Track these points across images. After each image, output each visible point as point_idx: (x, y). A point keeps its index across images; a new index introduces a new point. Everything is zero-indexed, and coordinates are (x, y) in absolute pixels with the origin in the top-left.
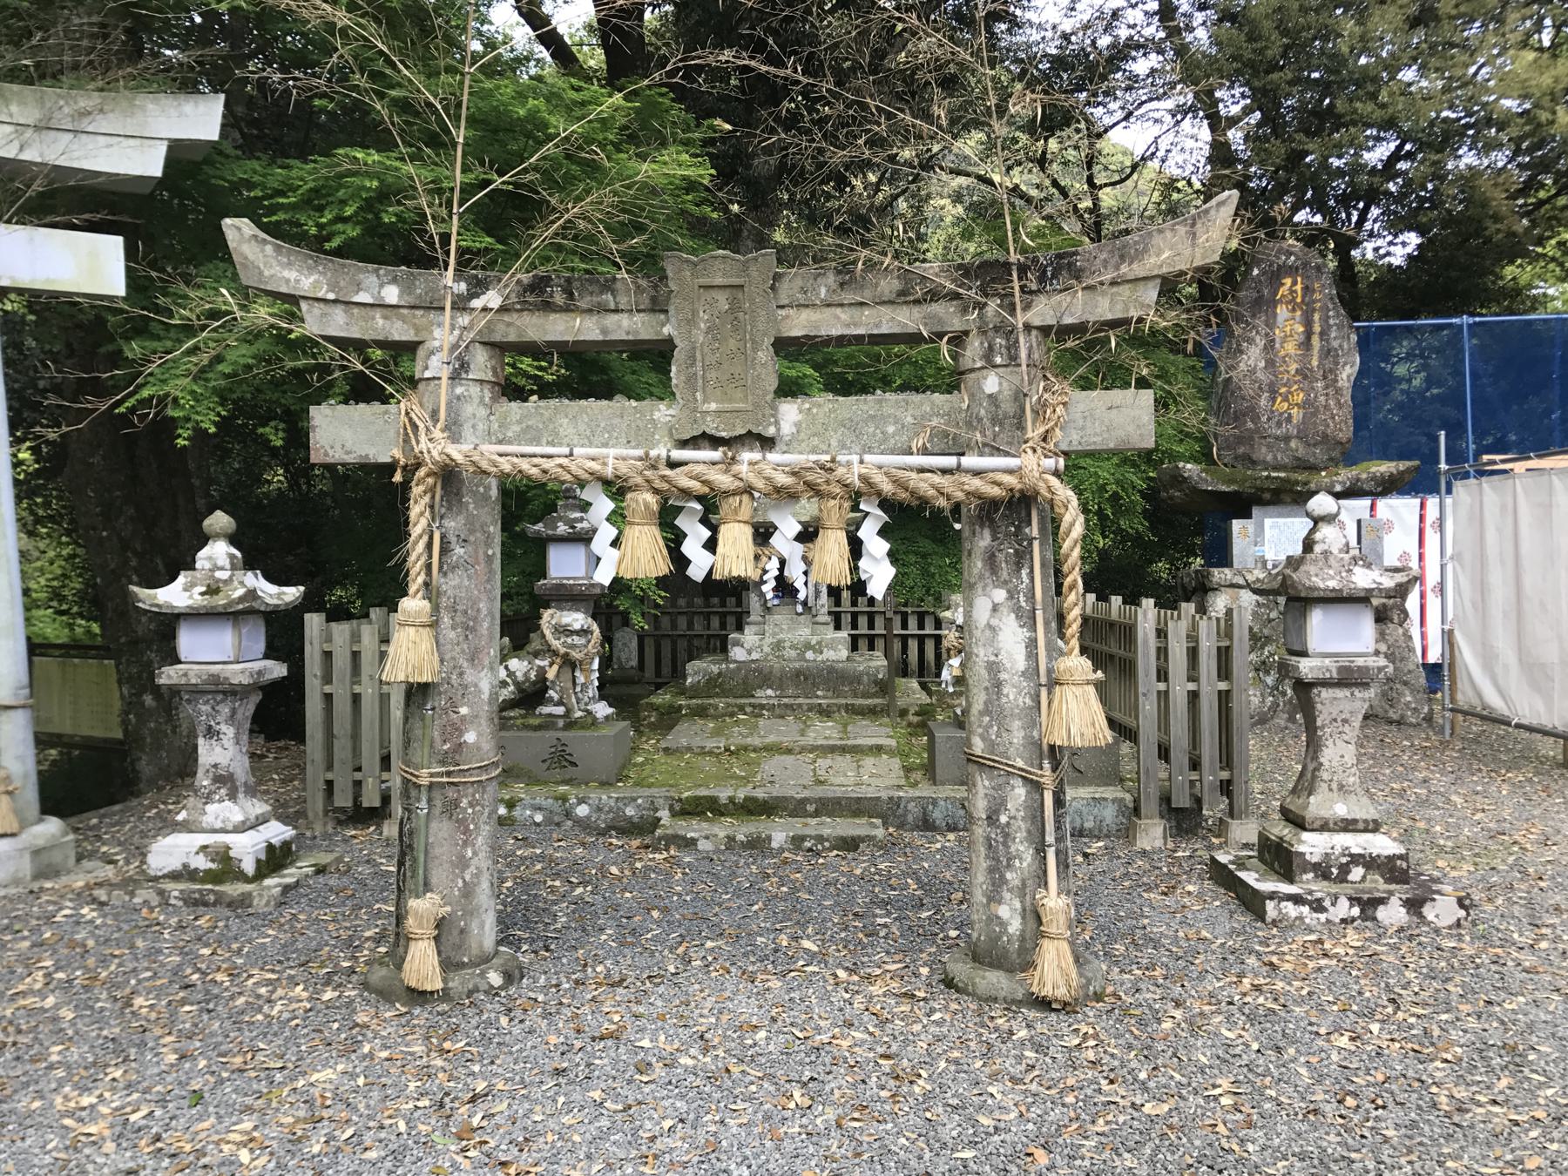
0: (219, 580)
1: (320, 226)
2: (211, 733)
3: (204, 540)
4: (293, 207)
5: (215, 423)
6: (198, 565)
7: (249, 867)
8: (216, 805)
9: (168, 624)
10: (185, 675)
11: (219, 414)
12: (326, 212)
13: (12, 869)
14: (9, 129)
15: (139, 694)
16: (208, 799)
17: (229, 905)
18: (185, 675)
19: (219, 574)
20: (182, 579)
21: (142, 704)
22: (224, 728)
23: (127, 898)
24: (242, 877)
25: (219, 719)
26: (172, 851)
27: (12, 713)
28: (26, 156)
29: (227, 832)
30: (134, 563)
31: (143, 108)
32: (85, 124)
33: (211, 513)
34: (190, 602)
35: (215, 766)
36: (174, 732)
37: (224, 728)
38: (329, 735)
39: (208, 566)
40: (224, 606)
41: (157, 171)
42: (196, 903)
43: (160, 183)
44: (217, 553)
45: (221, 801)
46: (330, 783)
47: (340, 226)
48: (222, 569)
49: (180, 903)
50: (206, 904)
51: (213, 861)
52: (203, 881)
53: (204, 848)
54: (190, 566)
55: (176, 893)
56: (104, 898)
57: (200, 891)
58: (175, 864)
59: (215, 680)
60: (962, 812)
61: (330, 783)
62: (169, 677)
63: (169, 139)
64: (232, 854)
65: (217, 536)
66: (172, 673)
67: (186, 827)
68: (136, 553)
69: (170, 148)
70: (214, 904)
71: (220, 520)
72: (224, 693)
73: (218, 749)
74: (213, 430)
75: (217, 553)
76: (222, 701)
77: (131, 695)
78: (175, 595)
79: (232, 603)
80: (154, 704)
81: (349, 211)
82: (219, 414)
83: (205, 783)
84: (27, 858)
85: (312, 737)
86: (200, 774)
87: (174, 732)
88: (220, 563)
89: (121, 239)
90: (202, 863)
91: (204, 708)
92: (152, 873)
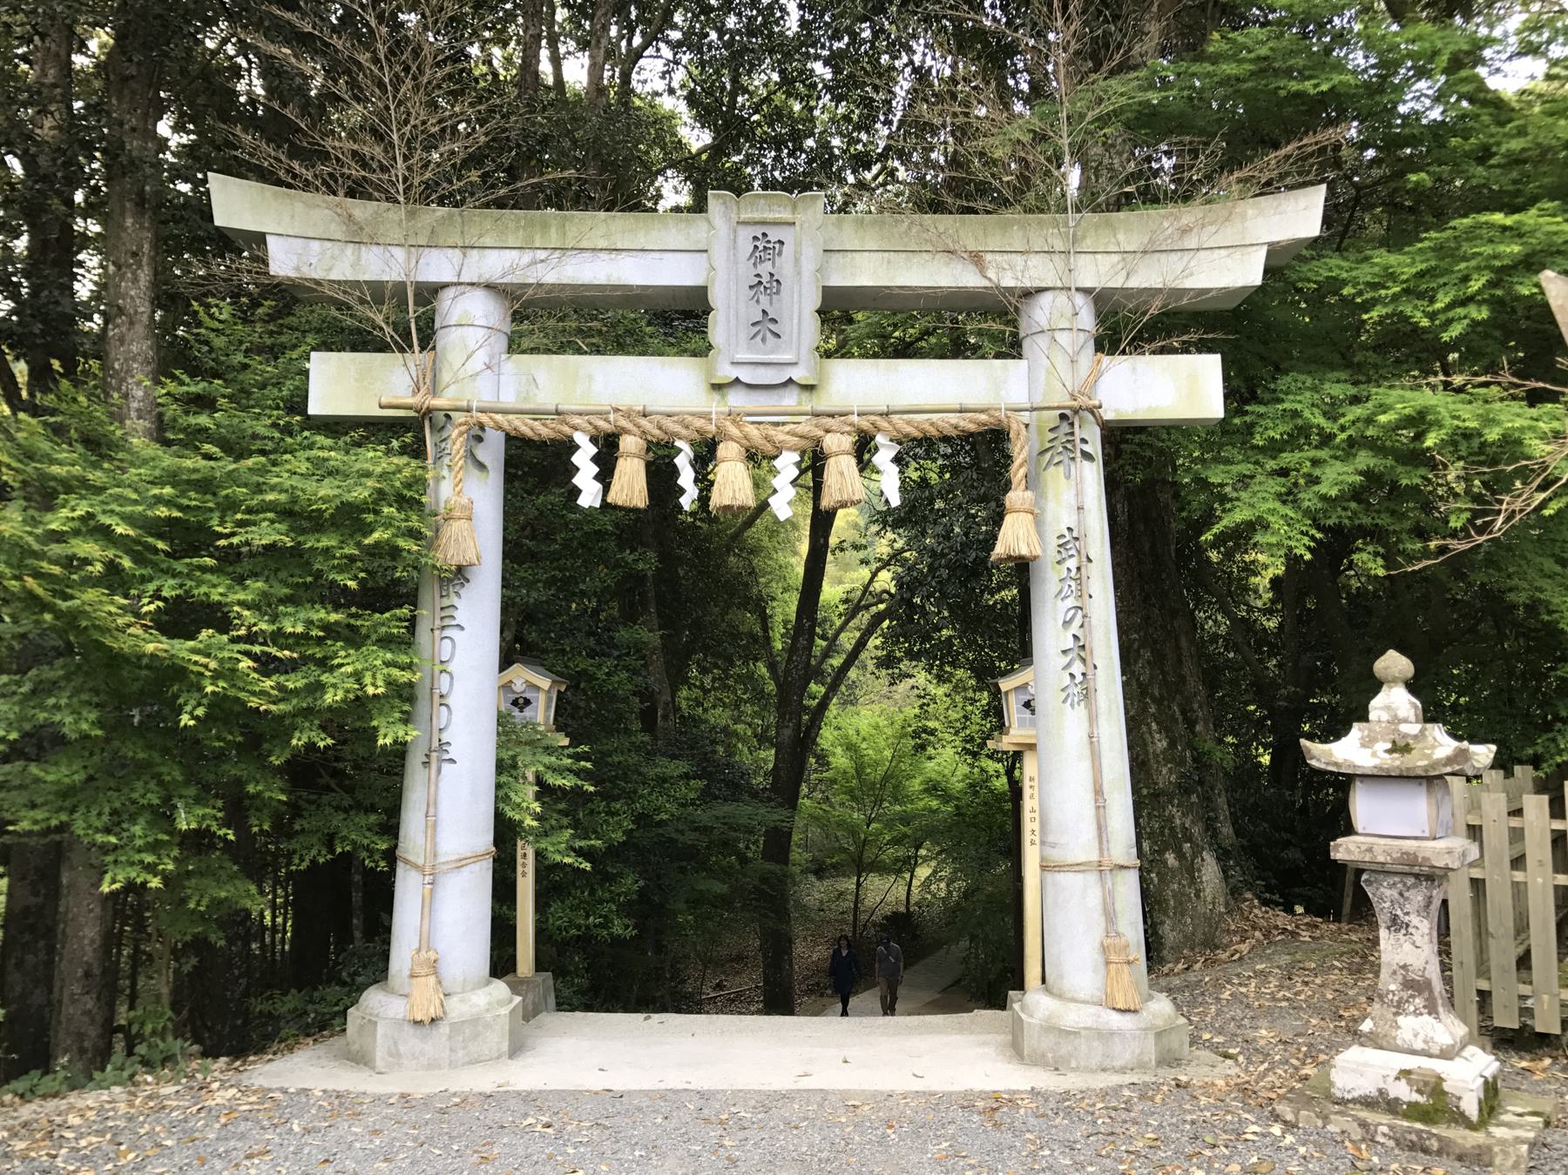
0: (1405, 736)
1: (1432, 316)
2: (1396, 924)
3: (1375, 686)
4: (1395, 298)
5: (1309, 548)
6: (1372, 716)
7: (1471, 1107)
8: (1411, 1018)
9: (1342, 782)
10: (1370, 850)
11: (1313, 538)
12: (1440, 296)
13: (1137, 1051)
14: (1116, 258)
15: (1161, 852)
16: (1399, 1008)
17: (1460, 1158)
18: (1370, 850)
19: (1404, 728)
20: (1357, 731)
21: (1165, 862)
22: (1414, 920)
23: (1320, 1123)
24: (1460, 1119)
25: (1408, 908)
26: (1359, 1070)
27: (1125, 873)
28: (1135, 283)
29: (1430, 1056)
30: (1153, 710)
31: (1244, 217)
32: (1191, 242)
33: (1382, 653)
34: (1376, 762)
35: (1404, 967)
36: (1198, 896)
37: (1414, 920)
38: (1481, 932)
39: (1385, 717)
40: (1426, 768)
41: (1256, 278)
42: (1412, 1147)
43: (1260, 289)
44: (1394, 703)
45: (1416, 1013)
46: (1484, 996)
47: (1460, 311)
48: (1406, 721)
49: (1391, 1143)
50: (1426, 1151)
51: (1419, 1091)
52: (1406, 1116)
53: (1405, 1074)
54: (1364, 717)
55: (1385, 1129)
56: (1290, 1117)
57: (1419, 1132)
58: (1366, 1086)
59: (1410, 860)
60: (367, 803)
61: (1484, 996)
62: (1348, 851)
63: (1270, 244)
64: (1446, 1087)
65: (1394, 681)
66: (1352, 847)
67: (1374, 1041)
68: (1154, 700)
69: (1269, 253)
70: (1439, 1153)
71: (1394, 663)
72: (1417, 876)
73: (1407, 947)
74: (1308, 557)
75: (1394, 703)
76: (1414, 886)
77: (1153, 852)
78: (1348, 751)
79: (1434, 765)
80: (1176, 864)
81: (1475, 285)
82: (1313, 538)
83: (1392, 987)
84: (1151, 1039)
85: (1460, 932)
86: (1384, 974)
87: (1198, 896)
88: (1402, 714)
89: (1218, 357)
90: (1404, 1092)
91: (1388, 892)
92: (1339, 1094)
